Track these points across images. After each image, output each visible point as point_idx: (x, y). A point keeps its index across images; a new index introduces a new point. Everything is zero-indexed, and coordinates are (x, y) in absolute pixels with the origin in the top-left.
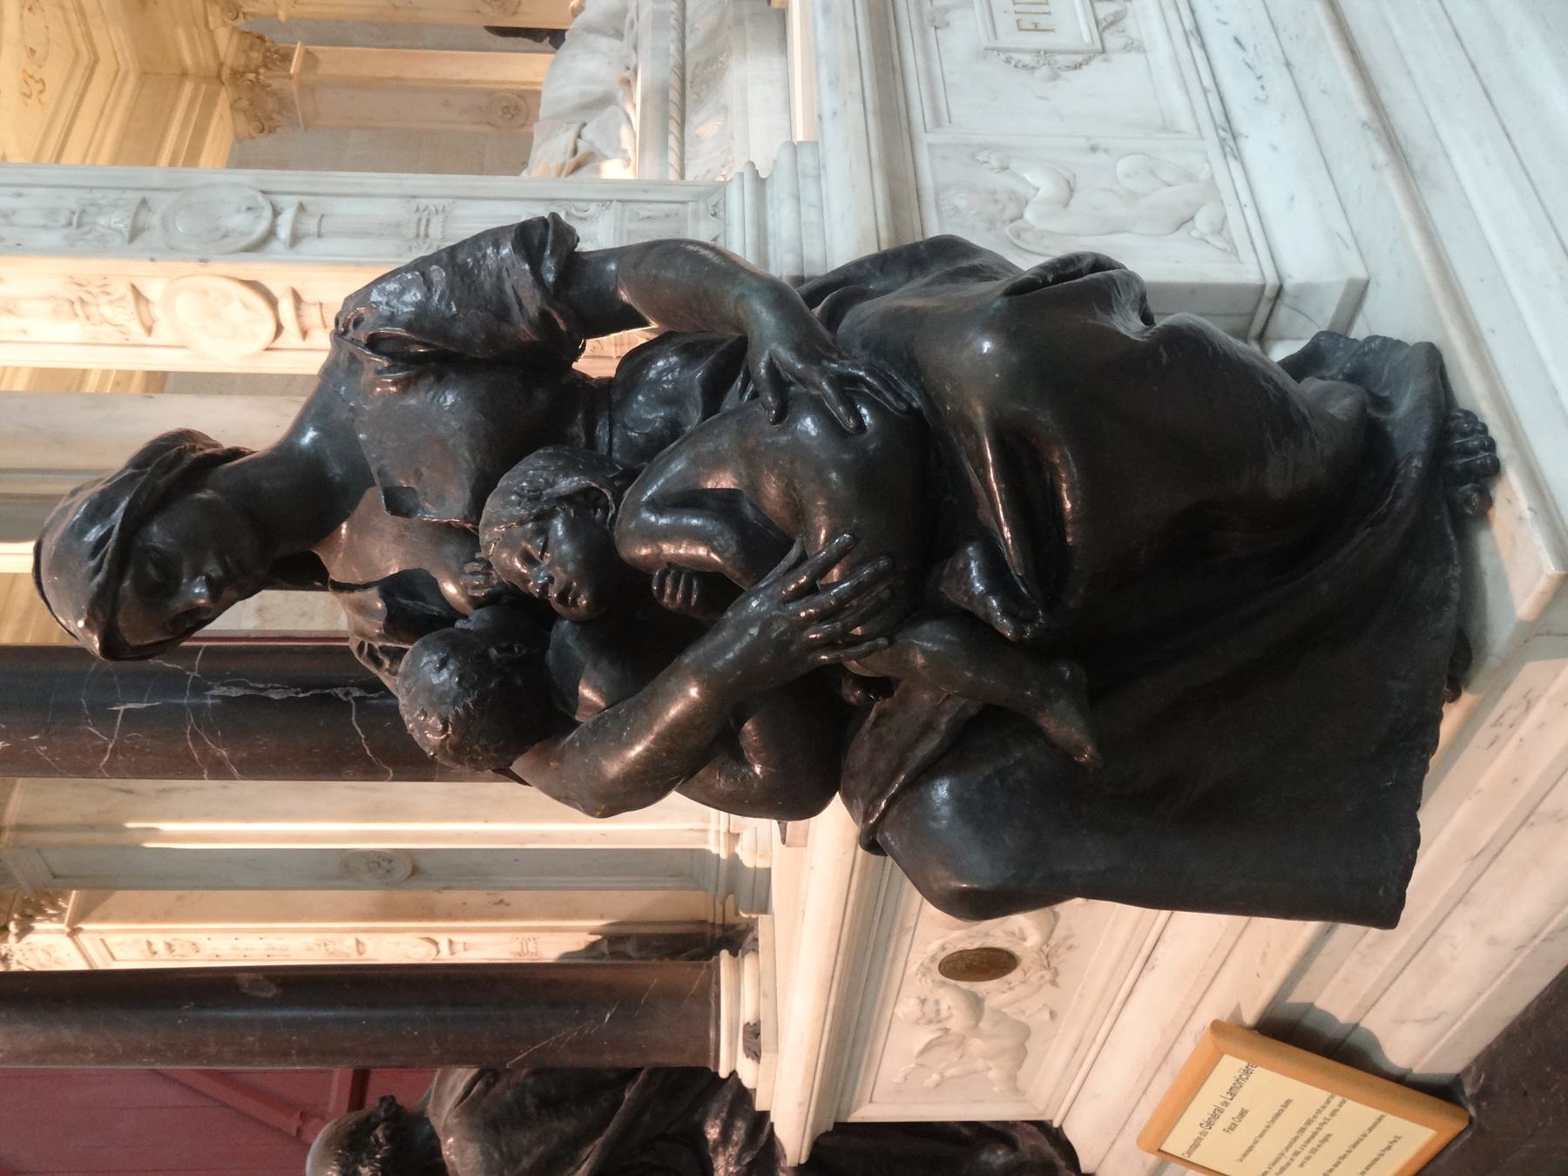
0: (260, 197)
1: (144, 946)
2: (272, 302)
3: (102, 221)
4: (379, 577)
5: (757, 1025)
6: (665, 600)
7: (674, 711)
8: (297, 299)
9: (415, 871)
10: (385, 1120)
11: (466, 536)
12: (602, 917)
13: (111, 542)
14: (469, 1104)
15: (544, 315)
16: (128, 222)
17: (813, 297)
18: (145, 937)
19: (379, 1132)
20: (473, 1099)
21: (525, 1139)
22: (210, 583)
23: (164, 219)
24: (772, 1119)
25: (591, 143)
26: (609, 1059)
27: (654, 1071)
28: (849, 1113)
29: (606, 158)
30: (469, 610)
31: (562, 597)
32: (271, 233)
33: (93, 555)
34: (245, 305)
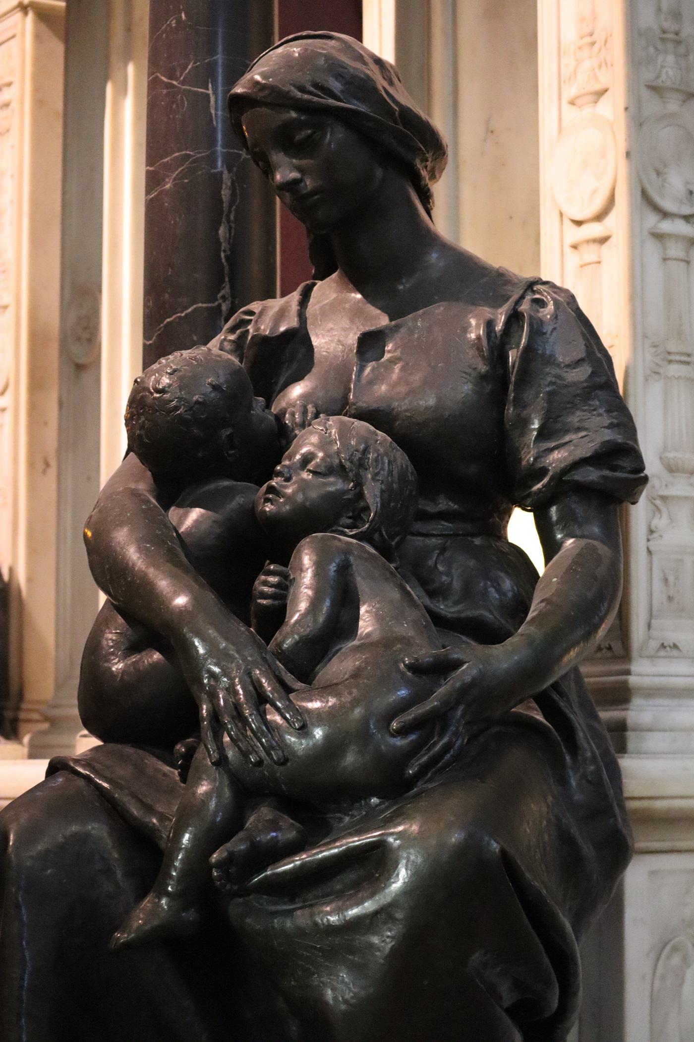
1: (7, 80)
2: (600, 217)
3: (670, 58)
4: (310, 327)
6: (263, 577)
7: (163, 584)
8: (603, 240)
9: (80, 368)
11: (339, 406)
12: (29, 580)
13: (331, 102)
15: (544, 471)
16: (668, 84)
18: (16, 79)
22: (296, 182)
23: (672, 115)
30: (274, 409)
31: (271, 489)
32: (665, 215)
33: (316, 85)
34: (594, 192)
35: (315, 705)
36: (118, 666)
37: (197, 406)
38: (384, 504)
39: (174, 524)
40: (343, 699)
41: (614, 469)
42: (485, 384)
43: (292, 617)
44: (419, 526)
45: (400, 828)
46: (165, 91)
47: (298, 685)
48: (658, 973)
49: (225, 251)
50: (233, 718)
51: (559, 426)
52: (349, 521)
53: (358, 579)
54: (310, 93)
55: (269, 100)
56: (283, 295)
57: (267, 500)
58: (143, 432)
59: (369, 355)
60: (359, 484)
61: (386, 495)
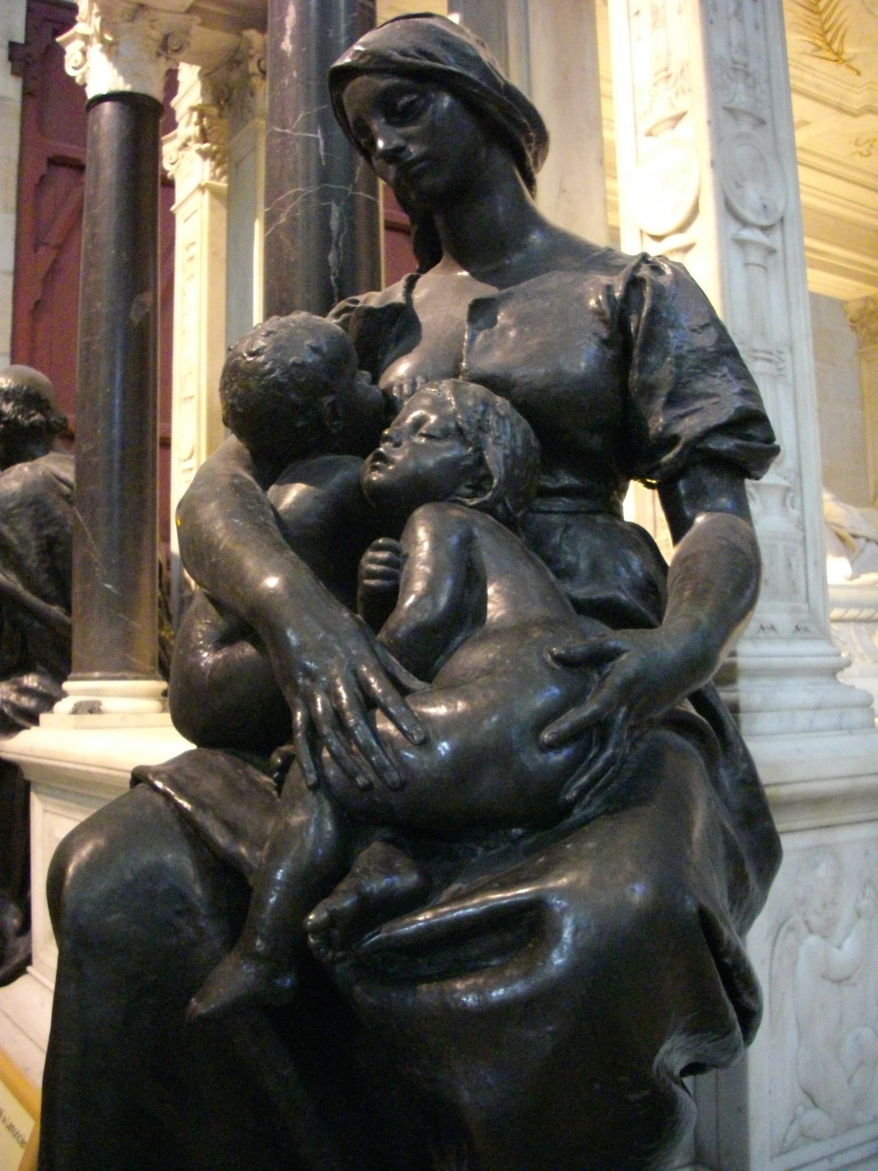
0: (778, 217)
2: (682, 229)
3: (741, 86)
5: (99, 711)
7: (250, 564)
10: (48, 422)
14: (53, 482)
16: (742, 107)
17: (700, 700)
19: (38, 417)
20: (55, 485)
21: (24, 527)
22: (400, 149)
24: (34, 729)
25: (862, 551)
26: (77, 589)
27: (69, 628)
28: (36, 792)
29: (852, 563)
30: (382, 384)
35: (439, 710)
36: (207, 658)
37: (294, 368)
38: (508, 474)
39: (272, 502)
40: (476, 703)
41: (749, 438)
42: (606, 349)
43: (404, 601)
44: (537, 503)
45: (564, 881)
46: (279, 140)
47: (416, 684)
48: (776, 956)
49: (334, 275)
50: (333, 728)
51: (688, 391)
52: (468, 491)
53: (484, 554)
54: (413, 56)
55: (372, 66)
56: (388, 284)
57: (375, 468)
58: (235, 401)
59: (480, 323)
60: (479, 450)
61: (510, 461)
